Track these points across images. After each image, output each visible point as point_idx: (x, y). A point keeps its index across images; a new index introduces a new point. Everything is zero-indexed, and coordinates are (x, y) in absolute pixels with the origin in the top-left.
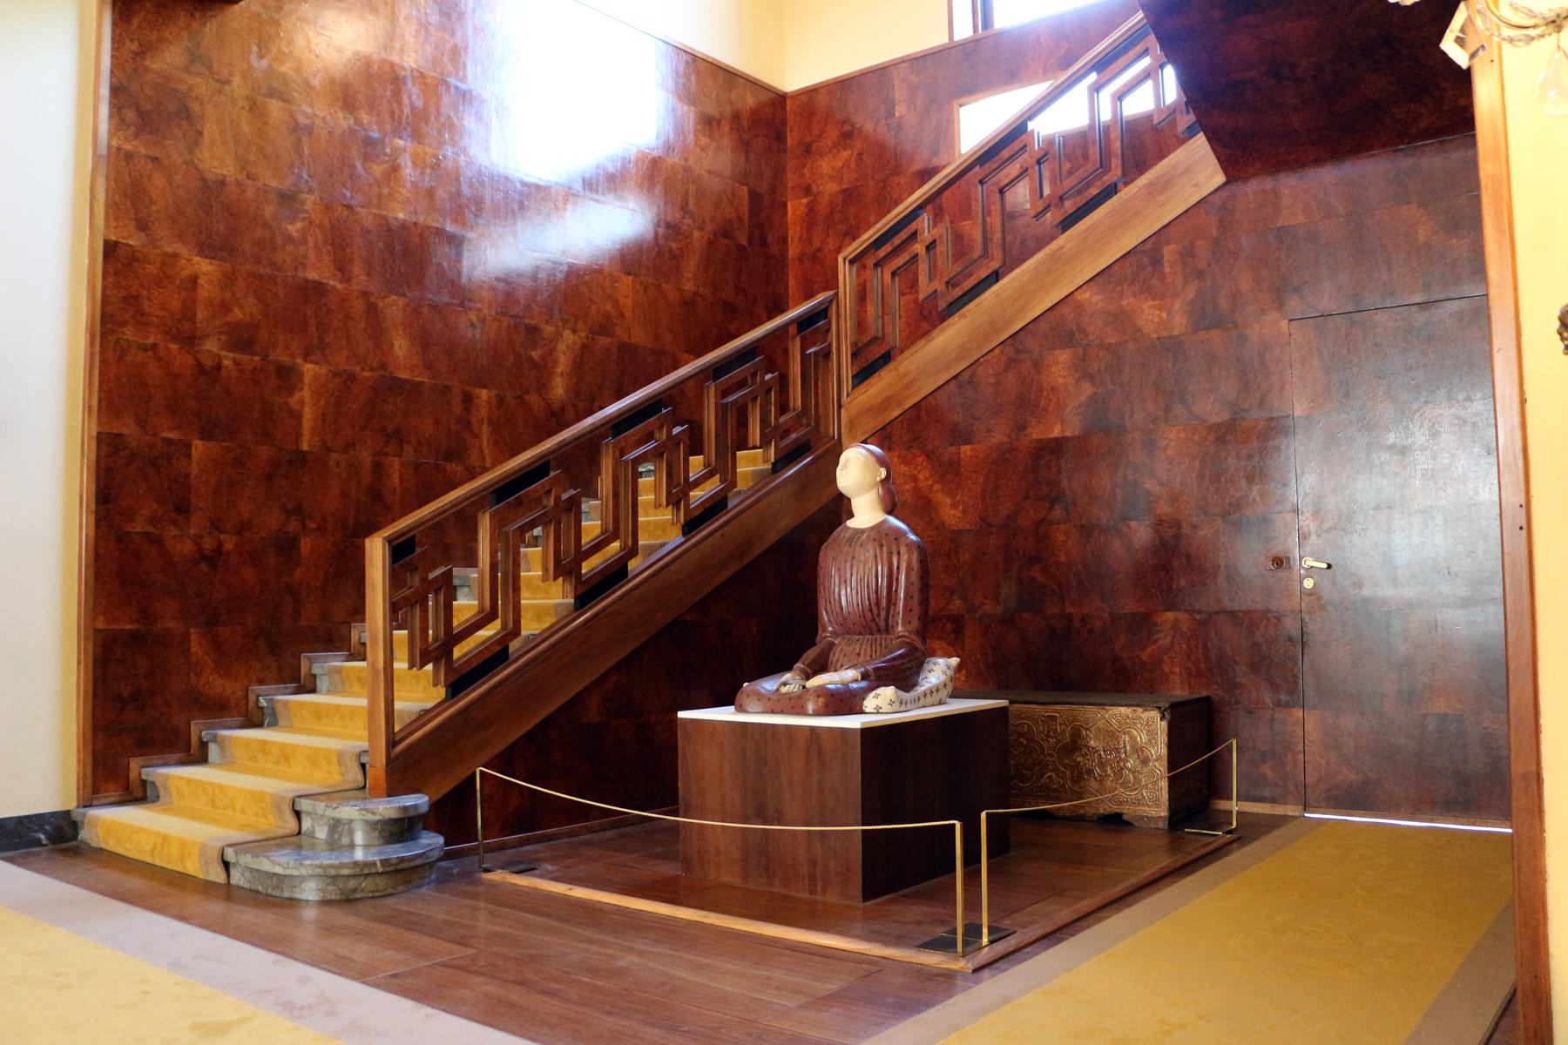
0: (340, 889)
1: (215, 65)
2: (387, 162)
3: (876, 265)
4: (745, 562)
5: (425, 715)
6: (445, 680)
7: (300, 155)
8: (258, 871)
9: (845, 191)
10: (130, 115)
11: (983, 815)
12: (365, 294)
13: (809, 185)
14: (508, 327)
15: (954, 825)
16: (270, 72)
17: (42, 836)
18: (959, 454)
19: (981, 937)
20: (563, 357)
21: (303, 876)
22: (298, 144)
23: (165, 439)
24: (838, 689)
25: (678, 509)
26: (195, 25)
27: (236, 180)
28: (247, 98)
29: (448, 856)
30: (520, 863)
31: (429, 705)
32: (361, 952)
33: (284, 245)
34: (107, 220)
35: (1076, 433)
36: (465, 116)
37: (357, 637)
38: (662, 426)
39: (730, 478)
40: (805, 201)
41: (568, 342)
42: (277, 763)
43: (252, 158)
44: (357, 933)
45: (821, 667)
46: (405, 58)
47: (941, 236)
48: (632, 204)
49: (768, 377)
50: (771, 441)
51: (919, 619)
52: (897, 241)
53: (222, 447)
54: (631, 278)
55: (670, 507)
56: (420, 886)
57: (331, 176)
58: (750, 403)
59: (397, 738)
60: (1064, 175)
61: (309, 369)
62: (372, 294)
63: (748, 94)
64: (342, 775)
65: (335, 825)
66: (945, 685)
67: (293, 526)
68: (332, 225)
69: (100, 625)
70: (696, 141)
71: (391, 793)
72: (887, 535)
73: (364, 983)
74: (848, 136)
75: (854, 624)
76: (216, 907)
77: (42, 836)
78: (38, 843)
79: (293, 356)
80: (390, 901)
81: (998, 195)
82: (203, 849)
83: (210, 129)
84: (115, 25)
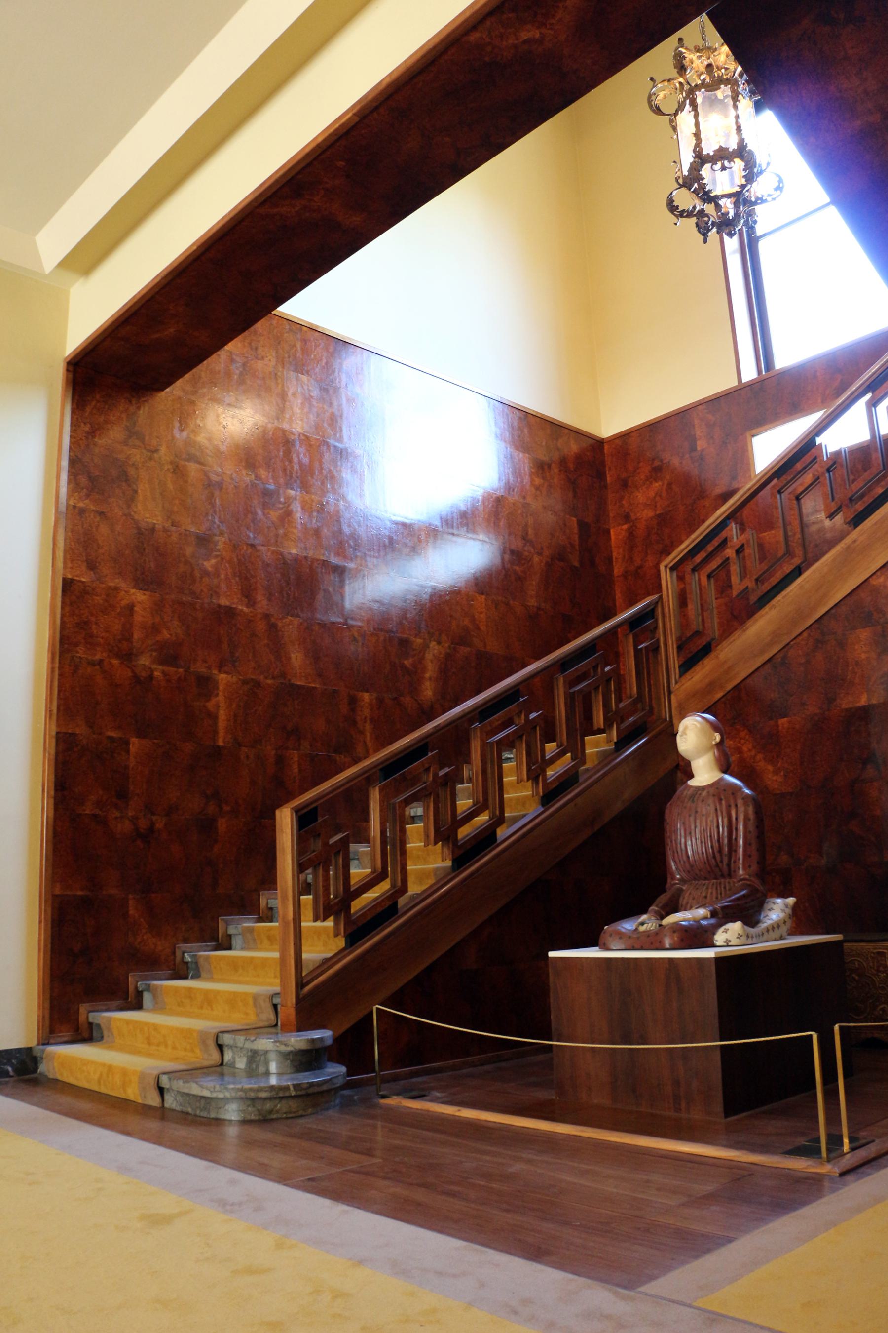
0: (258, 1110)
1: (147, 438)
2: (282, 508)
3: (694, 570)
4: (596, 828)
5: (326, 963)
6: (345, 932)
7: (213, 505)
8: (188, 1095)
9: (659, 516)
10: (83, 480)
11: (836, 1027)
12: (267, 616)
13: (628, 513)
14: (385, 640)
15: (811, 1036)
16: (189, 443)
17: (10, 1069)
18: (778, 726)
19: (842, 1145)
20: (430, 664)
21: (228, 1099)
22: (211, 498)
23: (110, 737)
24: (691, 925)
25: (537, 784)
26: (132, 409)
27: (164, 527)
28: (171, 463)
29: (348, 1085)
30: (412, 1090)
31: (329, 955)
32: (277, 1160)
33: (201, 578)
34: (65, 563)
35: (881, 701)
36: (343, 469)
37: (265, 903)
38: (521, 712)
39: (580, 755)
40: (625, 527)
41: (434, 650)
42: (201, 1007)
43: (175, 509)
44: (275, 1146)
45: (675, 908)
46: (294, 426)
47: (748, 541)
48: (481, 536)
49: (607, 669)
50: (612, 724)
51: (758, 863)
52: (710, 548)
53: (154, 743)
54: (484, 597)
55: (530, 781)
56: (327, 1109)
57: (237, 521)
58: (593, 692)
59: (305, 981)
60: (851, 482)
61: (223, 678)
62: (272, 615)
63: (572, 442)
64: (257, 1015)
65: (254, 1056)
66: (785, 922)
67: (211, 809)
68: (239, 561)
69: (57, 891)
70: (531, 482)
71: (301, 1027)
72: (725, 790)
73: (284, 1185)
74: (657, 471)
75: (700, 871)
76: (154, 1125)
77: (10, 1069)
78: (6, 1074)
79: (209, 668)
80: (301, 1121)
81: (795, 502)
82: (142, 1076)
83: (143, 488)
84: (73, 412)
